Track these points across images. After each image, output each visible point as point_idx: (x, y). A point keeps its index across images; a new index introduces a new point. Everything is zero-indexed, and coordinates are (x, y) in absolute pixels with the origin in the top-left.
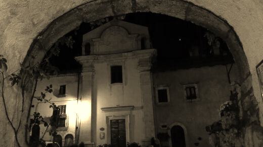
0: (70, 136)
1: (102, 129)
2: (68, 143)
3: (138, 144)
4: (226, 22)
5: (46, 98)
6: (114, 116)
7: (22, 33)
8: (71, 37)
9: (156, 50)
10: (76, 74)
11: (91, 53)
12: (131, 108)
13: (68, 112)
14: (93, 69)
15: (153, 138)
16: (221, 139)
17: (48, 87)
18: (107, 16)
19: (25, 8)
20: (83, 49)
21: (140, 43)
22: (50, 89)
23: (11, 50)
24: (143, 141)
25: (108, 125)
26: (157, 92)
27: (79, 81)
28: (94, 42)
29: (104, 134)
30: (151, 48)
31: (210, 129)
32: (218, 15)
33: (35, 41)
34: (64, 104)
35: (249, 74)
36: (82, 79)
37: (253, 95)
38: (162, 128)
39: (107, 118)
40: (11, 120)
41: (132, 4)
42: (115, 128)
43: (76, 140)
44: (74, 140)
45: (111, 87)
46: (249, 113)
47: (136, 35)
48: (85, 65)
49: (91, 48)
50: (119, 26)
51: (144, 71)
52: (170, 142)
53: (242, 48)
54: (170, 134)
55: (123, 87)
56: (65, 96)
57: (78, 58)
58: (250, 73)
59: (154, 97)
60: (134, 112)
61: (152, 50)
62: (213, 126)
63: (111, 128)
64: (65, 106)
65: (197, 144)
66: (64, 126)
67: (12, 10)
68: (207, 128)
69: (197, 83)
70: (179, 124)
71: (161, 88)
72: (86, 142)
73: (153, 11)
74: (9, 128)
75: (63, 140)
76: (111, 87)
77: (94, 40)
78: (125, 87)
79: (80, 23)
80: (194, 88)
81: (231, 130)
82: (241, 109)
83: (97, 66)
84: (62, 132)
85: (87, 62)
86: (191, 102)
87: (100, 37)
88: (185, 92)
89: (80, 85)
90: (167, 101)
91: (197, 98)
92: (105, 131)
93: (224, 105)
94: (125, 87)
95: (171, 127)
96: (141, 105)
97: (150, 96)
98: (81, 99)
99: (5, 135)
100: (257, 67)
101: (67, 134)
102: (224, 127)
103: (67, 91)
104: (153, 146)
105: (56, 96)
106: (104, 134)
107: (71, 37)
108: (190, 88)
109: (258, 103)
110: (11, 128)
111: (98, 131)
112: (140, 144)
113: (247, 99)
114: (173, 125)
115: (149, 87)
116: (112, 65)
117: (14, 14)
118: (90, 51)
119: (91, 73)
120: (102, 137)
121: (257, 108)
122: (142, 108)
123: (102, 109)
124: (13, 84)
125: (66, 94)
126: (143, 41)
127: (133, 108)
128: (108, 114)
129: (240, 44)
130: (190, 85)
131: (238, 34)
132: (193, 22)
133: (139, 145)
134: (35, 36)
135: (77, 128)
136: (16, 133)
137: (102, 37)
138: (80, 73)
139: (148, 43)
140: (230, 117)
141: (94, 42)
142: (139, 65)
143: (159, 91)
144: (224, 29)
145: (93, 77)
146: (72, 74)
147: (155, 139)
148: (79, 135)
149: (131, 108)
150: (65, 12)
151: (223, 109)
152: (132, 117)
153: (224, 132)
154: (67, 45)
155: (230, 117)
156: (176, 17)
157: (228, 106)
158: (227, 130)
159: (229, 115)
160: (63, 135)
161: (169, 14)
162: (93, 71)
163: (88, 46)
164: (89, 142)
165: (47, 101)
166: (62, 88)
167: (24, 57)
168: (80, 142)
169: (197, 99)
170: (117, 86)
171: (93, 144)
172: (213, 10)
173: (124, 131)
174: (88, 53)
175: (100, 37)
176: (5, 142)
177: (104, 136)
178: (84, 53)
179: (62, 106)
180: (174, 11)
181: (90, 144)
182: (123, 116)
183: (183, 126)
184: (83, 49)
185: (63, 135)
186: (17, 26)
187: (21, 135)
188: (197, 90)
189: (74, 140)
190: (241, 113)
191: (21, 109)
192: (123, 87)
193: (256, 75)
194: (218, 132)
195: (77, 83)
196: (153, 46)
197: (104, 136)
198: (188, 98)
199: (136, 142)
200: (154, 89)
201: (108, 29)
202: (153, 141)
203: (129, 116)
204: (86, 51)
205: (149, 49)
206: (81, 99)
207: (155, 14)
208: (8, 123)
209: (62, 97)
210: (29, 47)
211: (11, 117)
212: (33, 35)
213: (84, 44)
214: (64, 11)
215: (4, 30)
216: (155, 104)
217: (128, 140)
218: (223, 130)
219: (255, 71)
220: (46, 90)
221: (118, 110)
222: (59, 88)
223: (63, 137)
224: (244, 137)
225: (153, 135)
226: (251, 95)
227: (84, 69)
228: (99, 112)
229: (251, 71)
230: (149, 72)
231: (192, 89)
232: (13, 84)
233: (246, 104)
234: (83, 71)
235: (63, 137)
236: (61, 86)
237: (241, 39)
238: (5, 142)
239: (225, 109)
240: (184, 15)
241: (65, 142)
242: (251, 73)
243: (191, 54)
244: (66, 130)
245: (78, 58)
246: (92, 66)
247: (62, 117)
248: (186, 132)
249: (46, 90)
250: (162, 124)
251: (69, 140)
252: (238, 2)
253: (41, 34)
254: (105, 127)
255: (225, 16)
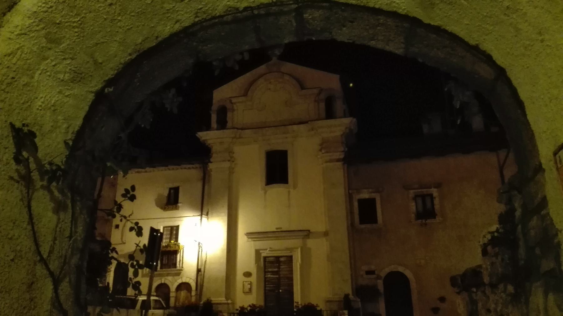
0: (184, 286)
1: (248, 274)
2: (181, 300)
3: (317, 306)
4: (488, 59)
5: (122, 212)
6: (272, 250)
7: (73, 81)
8: (173, 91)
9: (355, 120)
10: (197, 165)
11: (229, 125)
12: (305, 233)
13: (183, 239)
14: (231, 157)
15: (347, 296)
16: (480, 305)
17: (126, 190)
18: (247, 47)
19: (76, 30)
20: (214, 117)
21: (322, 105)
22: (132, 193)
23: (48, 114)
24: (328, 301)
25: (258, 268)
26: (356, 204)
27: (205, 179)
28: (235, 103)
29: (251, 284)
30: (345, 116)
31: (460, 282)
32: (472, 42)
33: (100, 96)
34: (176, 224)
35: (539, 169)
36: (210, 176)
37: (548, 214)
38: (365, 276)
39: (258, 252)
40: (45, 256)
41: (295, 24)
42: (273, 273)
43: (196, 294)
44: (193, 293)
45: (265, 193)
46: (538, 251)
47: (316, 91)
48: (216, 148)
49: (229, 115)
50: (283, 73)
51: (331, 161)
52: (382, 307)
53: (525, 115)
54: (381, 287)
55: (289, 192)
56: (177, 208)
57: (203, 135)
58: (541, 164)
59: (350, 212)
60: (311, 243)
61: (347, 122)
62: (464, 275)
63: (265, 272)
64: (178, 227)
65: (436, 310)
66: (175, 265)
67: (49, 33)
68: (453, 281)
69: (438, 186)
70: (401, 269)
71: (365, 195)
72: (215, 300)
73: (340, 38)
74: (40, 270)
75: (173, 294)
76: (265, 193)
77: (234, 100)
78: (292, 190)
79: (191, 61)
80: (431, 196)
81: (501, 286)
82: (521, 243)
83: (239, 151)
84: (170, 278)
85: (221, 143)
86: (426, 224)
87: (245, 95)
88: (413, 204)
89: (206, 187)
90: (375, 221)
91: (437, 218)
92: (253, 279)
93: (490, 233)
94: (292, 190)
95: (383, 274)
96: (324, 230)
97: (341, 212)
98: (207, 214)
99: (30, 285)
100: (555, 154)
101: (180, 281)
102: (486, 279)
103: (180, 200)
104: (346, 312)
105: (162, 208)
106: (251, 284)
107: (173, 91)
108: (423, 197)
109: (557, 230)
110: (45, 272)
111: (240, 277)
112: (321, 306)
113: (534, 222)
114: (387, 270)
115: (340, 192)
116: (269, 148)
117: (53, 41)
118: (226, 122)
119: (227, 165)
120: (247, 289)
121: (556, 241)
122: (326, 234)
123: (249, 235)
124: (50, 181)
125: (179, 205)
126: (329, 103)
127: (307, 234)
128: (260, 244)
129: (520, 105)
130: (425, 191)
131: (515, 83)
132: (420, 60)
133: (318, 309)
134: (100, 86)
135: (199, 271)
136: (56, 283)
137: (250, 93)
138: (207, 164)
139: (339, 106)
140: (500, 258)
141: (235, 103)
142: (321, 150)
143: (361, 201)
144: (485, 71)
145: (231, 171)
146: (191, 166)
147: (351, 297)
148: (202, 286)
149: (305, 233)
150: (160, 39)
151: (486, 240)
152: (306, 253)
153: (488, 291)
154: (167, 106)
155: (500, 258)
156: (388, 48)
157: (496, 234)
158: (493, 286)
159: (496, 255)
160: (173, 285)
161: (373, 43)
162: (231, 160)
163: (223, 112)
164: (223, 299)
165: (125, 217)
166: (172, 191)
167: (77, 128)
168: (204, 300)
169: (438, 219)
170: (277, 190)
171: (228, 304)
172: (462, 34)
173: (291, 279)
174: (222, 125)
175: (245, 95)
176: (32, 300)
177: (250, 289)
178: (214, 125)
179: (172, 228)
180: (381, 38)
181: (225, 304)
182: (287, 249)
183: (409, 274)
184: (214, 117)
185: (173, 283)
186: (61, 66)
187: (65, 287)
188: (437, 202)
189: (193, 293)
190: (522, 252)
191: (67, 233)
192: (289, 192)
193: (554, 169)
194: (475, 290)
195: (200, 185)
196: (350, 113)
197: (250, 289)
198: (419, 216)
199: (314, 302)
200: (350, 197)
201: (261, 80)
202: (346, 302)
203: (299, 250)
204: (218, 122)
205: (341, 117)
206: (207, 214)
207: (342, 43)
208: (40, 261)
209: (172, 209)
210: (87, 108)
211: (45, 250)
212: (96, 85)
213: (215, 107)
214: (157, 37)
215: (34, 73)
216: (351, 227)
217: (298, 298)
218: (484, 284)
219: (552, 163)
220: (124, 196)
221: (277, 238)
222: (166, 193)
223: (173, 288)
224: (527, 303)
225: (348, 289)
226: (543, 213)
227: (214, 155)
228: (242, 240)
229: (543, 161)
230: (340, 164)
231: (428, 200)
232: (50, 181)
233: (532, 233)
234: (212, 160)
235: (173, 288)
236: (170, 189)
237: (523, 95)
238: (32, 300)
239: (489, 240)
240: (403, 46)
241: (177, 298)
242: (544, 166)
243: (426, 129)
244: (179, 273)
245: (203, 135)
246: (230, 152)
247: (172, 249)
248: (413, 285)
249: (124, 196)
250: (365, 268)
251: (183, 294)
252: (514, 16)
253: (109, 83)
254: (252, 268)
255: (488, 46)
